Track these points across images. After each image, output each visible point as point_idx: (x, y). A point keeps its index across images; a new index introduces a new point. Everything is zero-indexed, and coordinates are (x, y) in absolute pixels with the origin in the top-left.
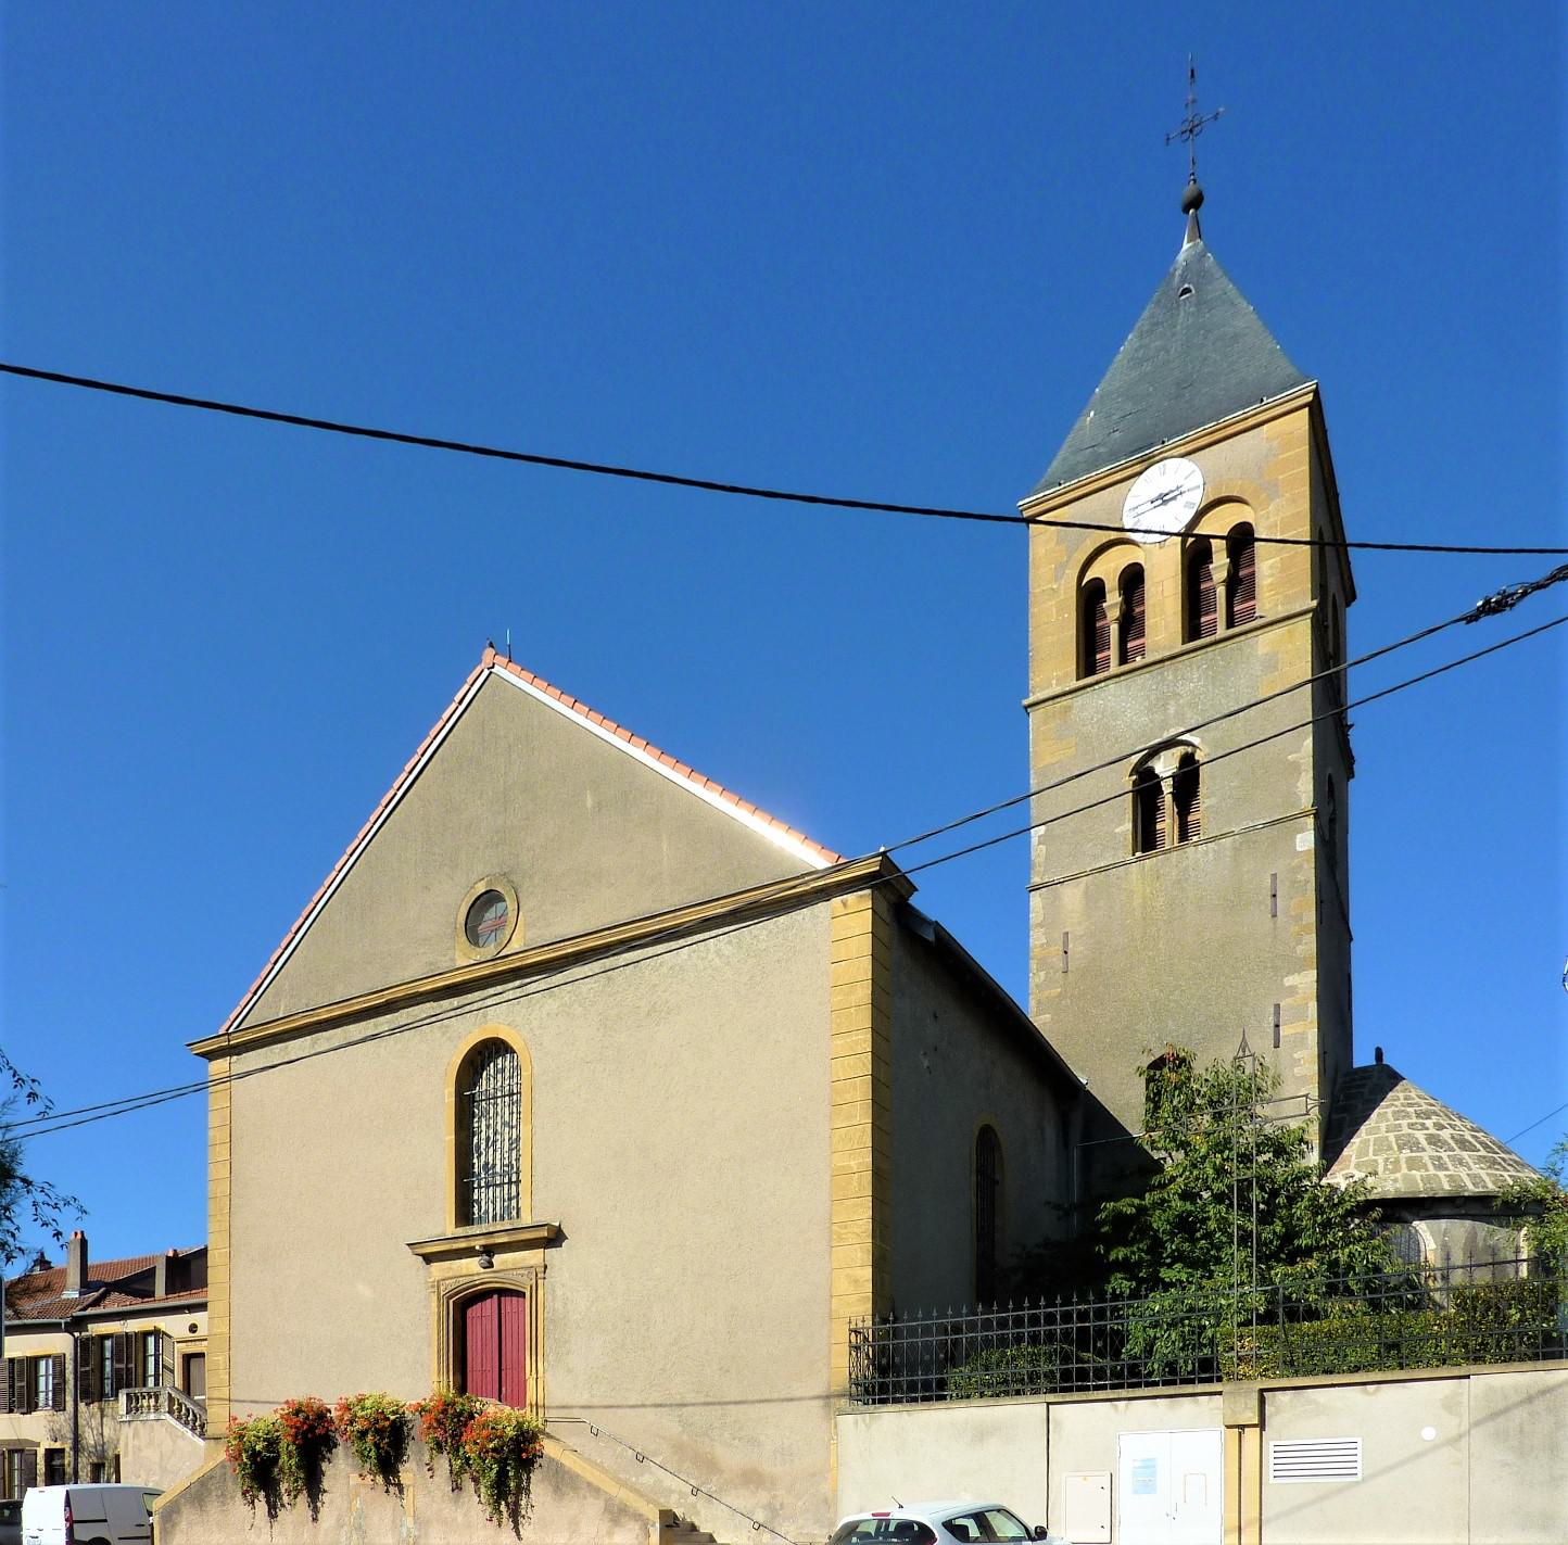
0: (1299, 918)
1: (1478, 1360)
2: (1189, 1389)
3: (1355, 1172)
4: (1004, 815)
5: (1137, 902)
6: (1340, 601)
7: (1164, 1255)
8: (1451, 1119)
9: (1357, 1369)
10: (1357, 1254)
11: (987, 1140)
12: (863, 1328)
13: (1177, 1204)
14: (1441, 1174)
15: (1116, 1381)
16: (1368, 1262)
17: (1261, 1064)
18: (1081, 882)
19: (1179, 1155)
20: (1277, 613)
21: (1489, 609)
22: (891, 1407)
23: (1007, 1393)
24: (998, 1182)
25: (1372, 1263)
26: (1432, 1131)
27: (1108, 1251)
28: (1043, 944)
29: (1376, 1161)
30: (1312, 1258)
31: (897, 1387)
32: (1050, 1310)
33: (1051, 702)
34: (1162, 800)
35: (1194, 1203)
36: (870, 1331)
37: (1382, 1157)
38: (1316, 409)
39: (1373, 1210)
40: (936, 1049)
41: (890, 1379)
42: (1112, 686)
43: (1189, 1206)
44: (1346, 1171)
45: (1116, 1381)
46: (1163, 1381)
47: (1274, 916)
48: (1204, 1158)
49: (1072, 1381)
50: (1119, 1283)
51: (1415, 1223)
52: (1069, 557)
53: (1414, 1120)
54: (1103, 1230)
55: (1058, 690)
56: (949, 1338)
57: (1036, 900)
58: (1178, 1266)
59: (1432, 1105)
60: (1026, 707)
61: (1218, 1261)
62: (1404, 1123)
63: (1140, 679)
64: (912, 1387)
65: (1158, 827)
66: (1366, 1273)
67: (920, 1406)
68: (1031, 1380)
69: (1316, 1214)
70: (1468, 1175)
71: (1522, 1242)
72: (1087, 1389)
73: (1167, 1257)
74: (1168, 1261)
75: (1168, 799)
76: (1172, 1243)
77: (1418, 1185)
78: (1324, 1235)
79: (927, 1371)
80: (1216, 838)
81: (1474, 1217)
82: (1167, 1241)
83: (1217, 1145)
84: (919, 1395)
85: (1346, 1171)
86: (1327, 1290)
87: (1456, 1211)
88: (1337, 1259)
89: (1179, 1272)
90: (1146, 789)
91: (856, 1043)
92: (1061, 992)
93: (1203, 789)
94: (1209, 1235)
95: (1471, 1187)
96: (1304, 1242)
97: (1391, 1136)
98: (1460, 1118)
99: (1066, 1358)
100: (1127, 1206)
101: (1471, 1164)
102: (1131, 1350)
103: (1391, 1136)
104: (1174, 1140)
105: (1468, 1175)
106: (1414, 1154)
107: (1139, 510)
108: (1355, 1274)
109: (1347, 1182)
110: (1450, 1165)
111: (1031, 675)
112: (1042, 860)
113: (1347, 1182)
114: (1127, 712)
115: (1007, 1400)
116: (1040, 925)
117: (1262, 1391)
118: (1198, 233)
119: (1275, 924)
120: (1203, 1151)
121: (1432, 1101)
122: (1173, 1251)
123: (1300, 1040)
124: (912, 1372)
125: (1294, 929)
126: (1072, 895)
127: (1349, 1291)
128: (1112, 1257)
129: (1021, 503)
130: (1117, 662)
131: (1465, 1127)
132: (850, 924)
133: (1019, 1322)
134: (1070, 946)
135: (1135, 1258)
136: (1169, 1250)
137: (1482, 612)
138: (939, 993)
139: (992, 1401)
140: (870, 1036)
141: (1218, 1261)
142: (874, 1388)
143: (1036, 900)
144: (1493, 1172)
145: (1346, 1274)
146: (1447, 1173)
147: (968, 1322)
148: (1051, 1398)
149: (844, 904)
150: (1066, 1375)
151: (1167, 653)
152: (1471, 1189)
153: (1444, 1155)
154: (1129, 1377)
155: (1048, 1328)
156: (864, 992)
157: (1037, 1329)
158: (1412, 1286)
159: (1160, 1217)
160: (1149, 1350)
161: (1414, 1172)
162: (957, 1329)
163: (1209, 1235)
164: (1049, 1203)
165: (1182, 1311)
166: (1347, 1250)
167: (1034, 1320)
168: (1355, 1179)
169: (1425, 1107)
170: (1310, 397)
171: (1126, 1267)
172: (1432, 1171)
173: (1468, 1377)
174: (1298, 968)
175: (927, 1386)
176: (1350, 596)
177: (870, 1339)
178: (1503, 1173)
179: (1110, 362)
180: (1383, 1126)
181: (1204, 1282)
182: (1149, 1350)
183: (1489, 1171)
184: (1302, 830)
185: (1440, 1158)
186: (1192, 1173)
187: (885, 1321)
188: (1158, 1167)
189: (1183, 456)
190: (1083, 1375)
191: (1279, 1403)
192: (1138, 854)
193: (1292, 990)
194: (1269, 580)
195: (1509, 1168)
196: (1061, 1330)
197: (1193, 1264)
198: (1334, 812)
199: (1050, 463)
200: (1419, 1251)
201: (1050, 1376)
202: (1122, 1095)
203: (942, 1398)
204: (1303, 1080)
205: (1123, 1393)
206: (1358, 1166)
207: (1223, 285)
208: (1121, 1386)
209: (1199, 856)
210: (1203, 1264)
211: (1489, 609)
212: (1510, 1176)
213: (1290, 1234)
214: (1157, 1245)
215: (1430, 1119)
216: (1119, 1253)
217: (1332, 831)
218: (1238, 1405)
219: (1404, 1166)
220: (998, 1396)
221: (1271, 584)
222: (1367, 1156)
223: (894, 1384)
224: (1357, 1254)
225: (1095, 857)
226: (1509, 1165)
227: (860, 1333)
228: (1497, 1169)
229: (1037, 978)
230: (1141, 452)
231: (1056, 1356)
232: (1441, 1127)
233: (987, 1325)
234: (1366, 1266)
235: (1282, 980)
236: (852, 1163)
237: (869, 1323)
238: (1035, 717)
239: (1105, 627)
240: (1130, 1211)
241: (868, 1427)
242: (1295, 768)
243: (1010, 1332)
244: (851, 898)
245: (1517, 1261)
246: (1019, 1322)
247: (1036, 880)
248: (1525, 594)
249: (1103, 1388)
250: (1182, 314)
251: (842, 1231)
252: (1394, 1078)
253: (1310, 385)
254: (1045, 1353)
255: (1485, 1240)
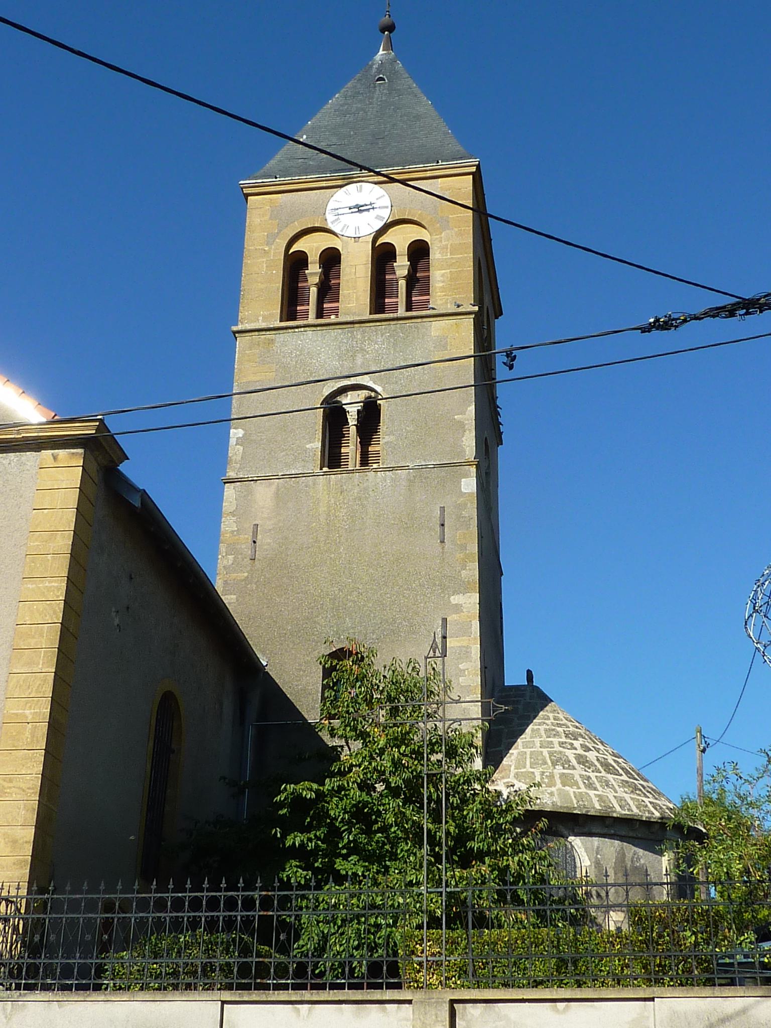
0: (463, 547)
1: (659, 982)
2: (377, 995)
3: (515, 782)
4: (209, 409)
5: (322, 509)
6: (491, 312)
7: (340, 846)
8: (594, 743)
9: (537, 984)
10: (526, 863)
11: (168, 706)
12: (17, 897)
13: (356, 793)
14: (592, 793)
15: (299, 981)
16: (536, 872)
17: (434, 669)
18: (270, 485)
19: (357, 745)
20: (446, 309)
21: (658, 325)
22: (39, 995)
23: (176, 987)
24: (173, 752)
25: (540, 874)
26: (580, 751)
27: (284, 836)
28: (233, 531)
29: (533, 773)
30: (484, 863)
31: (49, 971)
32: (230, 894)
33: (256, 333)
34: (348, 429)
35: (368, 794)
36: (24, 901)
37: (539, 770)
38: (477, 177)
39: (539, 820)
40: (128, 608)
41: (42, 960)
42: (310, 332)
43: (366, 798)
44: (506, 780)
45: (299, 981)
46: (330, 984)
47: (442, 542)
48: (382, 752)
49: (250, 978)
50: (294, 872)
51: (571, 838)
52: (280, 231)
53: (564, 739)
54: (281, 812)
55: (264, 325)
56: (221, 914)
57: (229, 491)
58: (354, 858)
59: (577, 727)
60: (234, 333)
61: (394, 857)
62: (556, 740)
63: (335, 332)
64: (67, 972)
65: (343, 450)
66: (534, 884)
67: (74, 996)
68: (205, 974)
69: (486, 818)
70: (615, 797)
71: (663, 864)
72: (266, 987)
73: (343, 848)
74: (344, 851)
75: (353, 430)
76: (350, 833)
77: (572, 801)
78: (496, 841)
79: (86, 954)
80: (393, 469)
81: (622, 838)
82: (344, 831)
83: (396, 739)
84: (310, 981)
85: (506, 780)
86: (510, 902)
87: (605, 831)
88: (508, 866)
89: (354, 865)
90: (334, 416)
91: (49, 589)
92: (247, 577)
93: (383, 427)
94: (385, 829)
95: (618, 809)
96: (475, 845)
97: (545, 752)
98: (602, 743)
99: (245, 951)
100: (307, 790)
101: (617, 787)
102: (303, 946)
103: (545, 752)
104: (354, 729)
105: (615, 797)
106: (565, 771)
107: (340, 211)
108: (524, 883)
109: (508, 790)
110: (598, 785)
111: (241, 308)
112: (239, 458)
113: (508, 790)
114: (321, 354)
115: (177, 995)
116: (232, 514)
117: (452, 1002)
118: (390, 46)
119: (443, 548)
120: (382, 743)
121: (577, 724)
122: (349, 842)
123: (465, 653)
124: (69, 954)
125: (459, 556)
126: (264, 493)
127: (517, 900)
128: (288, 843)
129: (242, 182)
130: (314, 316)
131: (607, 751)
132: (62, 476)
133: (196, 904)
134: (259, 537)
135: (311, 846)
136: (346, 841)
137: (653, 327)
138: (136, 560)
139: (159, 996)
140: (64, 585)
141: (394, 857)
142: (20, 969)
143: (229, 491)
144: (635, 796)
145: (515, 883)
146: (596, 792)
147: (122, 901)
148: (227, 995)
149: (55, 458)
150: (244, 970)
151: (357, 318)
152: (619, 811)
153: (593, 775)
154: (307, 978)
155: (245, 913)
156: (64, 542)
157: (216, 914)
158: (575, 900)
159: (337, 806)
160: (321, 950)
161: (567, 788)
162: (125, 907)
163: (385, 829)
164: (225, 778)
165: (358, 907)
166: (516, 859)
167: (213, 904)
168: (516, 788)
169: (572, 729)
170: (474, 169)
171: (303, 855)
172: (583, 789)
173: (652, 999)
174: (464, 589)
175: (84, 972)
176: (499, 313)
177: (23, 911)
178: (644, 799)
179: (321, 107)
180: (537, 741)
181: (380, 878)
182: (321, 950)
183: (632, 796)
184: (467, 476)
185: (589, 777)
186: (370, 764)
187: (42, 891)
188: (333, 754)
189: (376, 183)
190: (263, 970)
191: (469, 1015)
192: (325, 469)
193: (458, 608)
194: (441, 285)
195: (648, 794)
196: (242, 917)
197: (368, 857)
198: (489, 466)
199: (267, 162)
200: (575, 867)
201: (226, 969)
202: (299, 679)
203: (97, 988)
204: (468, 689)
205: (307, 995)
206: (517, 776)
207: (407, 82)
208: (303, 987)
209: (378, 480)
210: (378, 858)
211: (658, 325)
212: (650, 803)
213: (462, 837)
214: (334, 834)
215: (577, 739)
216: (295, 839)
217: (488, 482)
218: (428, 1016)
219: (558, 782)
220: (165, 989)
221: (443, 287)
222: (525, 767)
223: (46, 967)
224: (526, 863)
225: (288, 465)
226: (648, 792)
227: (12, 902)
228: (639, 795)
229: (225, 560)
230: (348, 166)
231: (235, 946)
232: (588, 749)
233: (160, 905)
234: (534, 876)
235: (449, 598)
236: (27, 712)
237: (24, 892)
238: (241, 342)
239: (307, 285)
240: (310, 795)
241: (8, 1018)
242: (461, 425)
243: (186, 915)
244: (62, 453)
245: (607, 885)
246: (196, 904)
247: (231, 474)
248: (685, 321)
249: (285, 987)
250: (377, 92)
251: (6, 785)
252: (544, 700)
253: (475, 162)
254: (222, 943)
255: (632, 861)
